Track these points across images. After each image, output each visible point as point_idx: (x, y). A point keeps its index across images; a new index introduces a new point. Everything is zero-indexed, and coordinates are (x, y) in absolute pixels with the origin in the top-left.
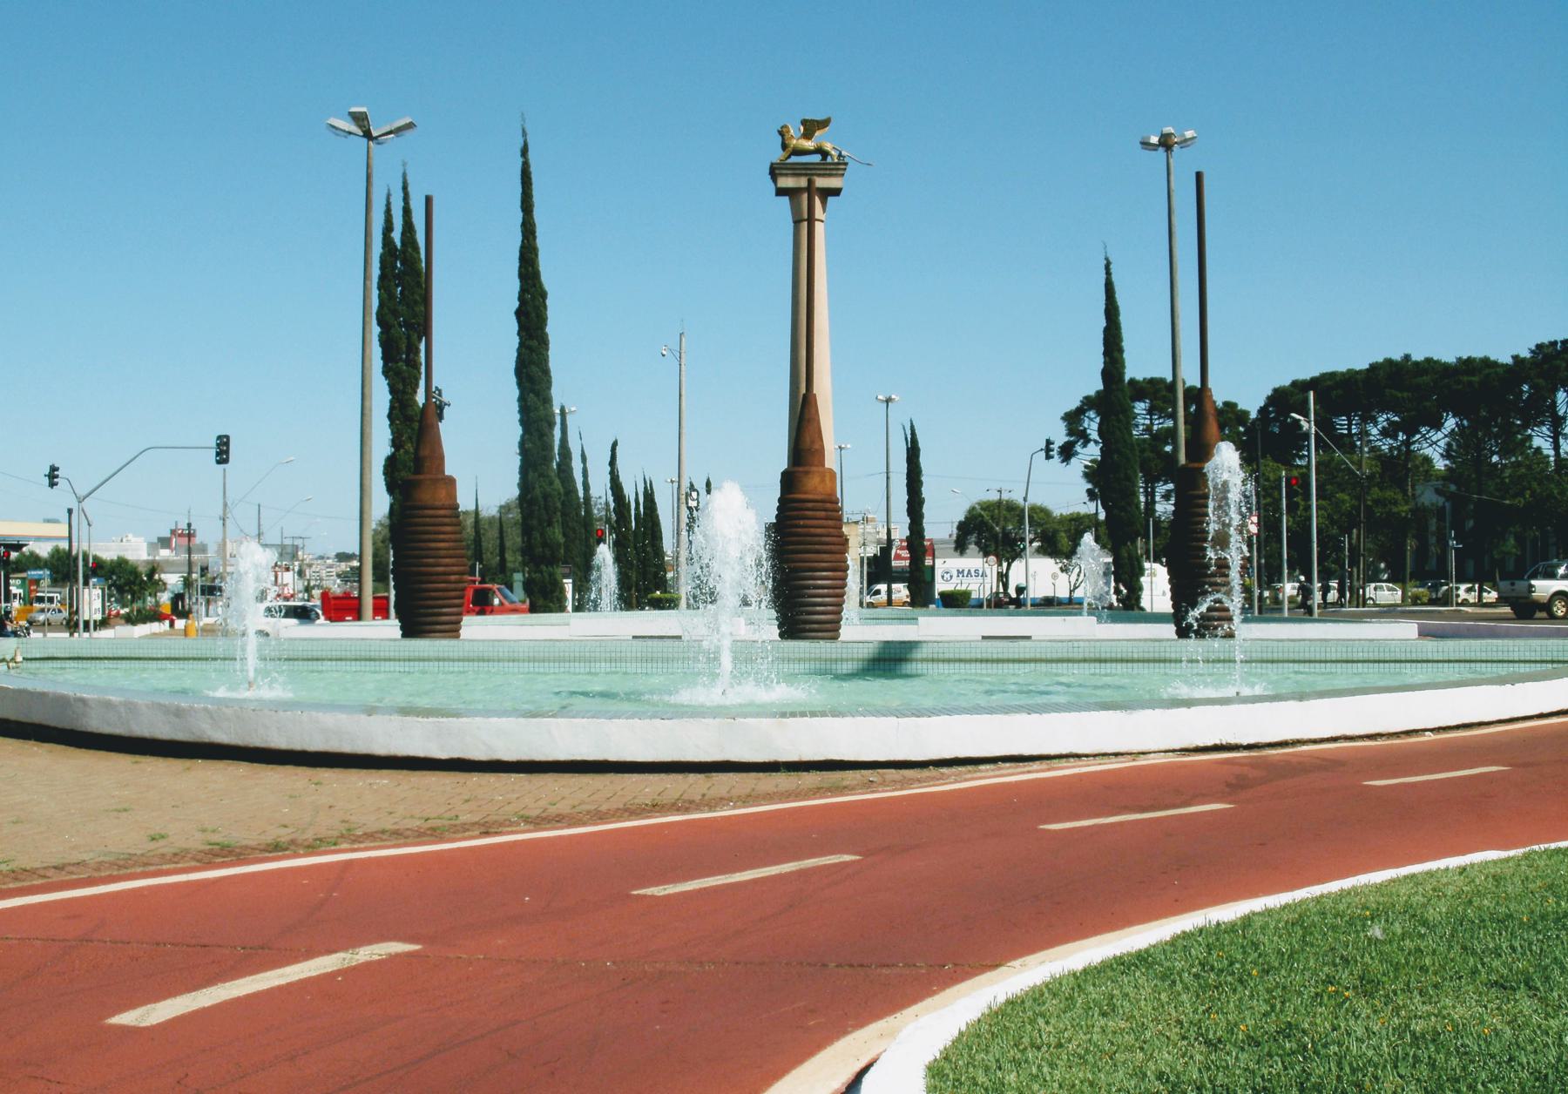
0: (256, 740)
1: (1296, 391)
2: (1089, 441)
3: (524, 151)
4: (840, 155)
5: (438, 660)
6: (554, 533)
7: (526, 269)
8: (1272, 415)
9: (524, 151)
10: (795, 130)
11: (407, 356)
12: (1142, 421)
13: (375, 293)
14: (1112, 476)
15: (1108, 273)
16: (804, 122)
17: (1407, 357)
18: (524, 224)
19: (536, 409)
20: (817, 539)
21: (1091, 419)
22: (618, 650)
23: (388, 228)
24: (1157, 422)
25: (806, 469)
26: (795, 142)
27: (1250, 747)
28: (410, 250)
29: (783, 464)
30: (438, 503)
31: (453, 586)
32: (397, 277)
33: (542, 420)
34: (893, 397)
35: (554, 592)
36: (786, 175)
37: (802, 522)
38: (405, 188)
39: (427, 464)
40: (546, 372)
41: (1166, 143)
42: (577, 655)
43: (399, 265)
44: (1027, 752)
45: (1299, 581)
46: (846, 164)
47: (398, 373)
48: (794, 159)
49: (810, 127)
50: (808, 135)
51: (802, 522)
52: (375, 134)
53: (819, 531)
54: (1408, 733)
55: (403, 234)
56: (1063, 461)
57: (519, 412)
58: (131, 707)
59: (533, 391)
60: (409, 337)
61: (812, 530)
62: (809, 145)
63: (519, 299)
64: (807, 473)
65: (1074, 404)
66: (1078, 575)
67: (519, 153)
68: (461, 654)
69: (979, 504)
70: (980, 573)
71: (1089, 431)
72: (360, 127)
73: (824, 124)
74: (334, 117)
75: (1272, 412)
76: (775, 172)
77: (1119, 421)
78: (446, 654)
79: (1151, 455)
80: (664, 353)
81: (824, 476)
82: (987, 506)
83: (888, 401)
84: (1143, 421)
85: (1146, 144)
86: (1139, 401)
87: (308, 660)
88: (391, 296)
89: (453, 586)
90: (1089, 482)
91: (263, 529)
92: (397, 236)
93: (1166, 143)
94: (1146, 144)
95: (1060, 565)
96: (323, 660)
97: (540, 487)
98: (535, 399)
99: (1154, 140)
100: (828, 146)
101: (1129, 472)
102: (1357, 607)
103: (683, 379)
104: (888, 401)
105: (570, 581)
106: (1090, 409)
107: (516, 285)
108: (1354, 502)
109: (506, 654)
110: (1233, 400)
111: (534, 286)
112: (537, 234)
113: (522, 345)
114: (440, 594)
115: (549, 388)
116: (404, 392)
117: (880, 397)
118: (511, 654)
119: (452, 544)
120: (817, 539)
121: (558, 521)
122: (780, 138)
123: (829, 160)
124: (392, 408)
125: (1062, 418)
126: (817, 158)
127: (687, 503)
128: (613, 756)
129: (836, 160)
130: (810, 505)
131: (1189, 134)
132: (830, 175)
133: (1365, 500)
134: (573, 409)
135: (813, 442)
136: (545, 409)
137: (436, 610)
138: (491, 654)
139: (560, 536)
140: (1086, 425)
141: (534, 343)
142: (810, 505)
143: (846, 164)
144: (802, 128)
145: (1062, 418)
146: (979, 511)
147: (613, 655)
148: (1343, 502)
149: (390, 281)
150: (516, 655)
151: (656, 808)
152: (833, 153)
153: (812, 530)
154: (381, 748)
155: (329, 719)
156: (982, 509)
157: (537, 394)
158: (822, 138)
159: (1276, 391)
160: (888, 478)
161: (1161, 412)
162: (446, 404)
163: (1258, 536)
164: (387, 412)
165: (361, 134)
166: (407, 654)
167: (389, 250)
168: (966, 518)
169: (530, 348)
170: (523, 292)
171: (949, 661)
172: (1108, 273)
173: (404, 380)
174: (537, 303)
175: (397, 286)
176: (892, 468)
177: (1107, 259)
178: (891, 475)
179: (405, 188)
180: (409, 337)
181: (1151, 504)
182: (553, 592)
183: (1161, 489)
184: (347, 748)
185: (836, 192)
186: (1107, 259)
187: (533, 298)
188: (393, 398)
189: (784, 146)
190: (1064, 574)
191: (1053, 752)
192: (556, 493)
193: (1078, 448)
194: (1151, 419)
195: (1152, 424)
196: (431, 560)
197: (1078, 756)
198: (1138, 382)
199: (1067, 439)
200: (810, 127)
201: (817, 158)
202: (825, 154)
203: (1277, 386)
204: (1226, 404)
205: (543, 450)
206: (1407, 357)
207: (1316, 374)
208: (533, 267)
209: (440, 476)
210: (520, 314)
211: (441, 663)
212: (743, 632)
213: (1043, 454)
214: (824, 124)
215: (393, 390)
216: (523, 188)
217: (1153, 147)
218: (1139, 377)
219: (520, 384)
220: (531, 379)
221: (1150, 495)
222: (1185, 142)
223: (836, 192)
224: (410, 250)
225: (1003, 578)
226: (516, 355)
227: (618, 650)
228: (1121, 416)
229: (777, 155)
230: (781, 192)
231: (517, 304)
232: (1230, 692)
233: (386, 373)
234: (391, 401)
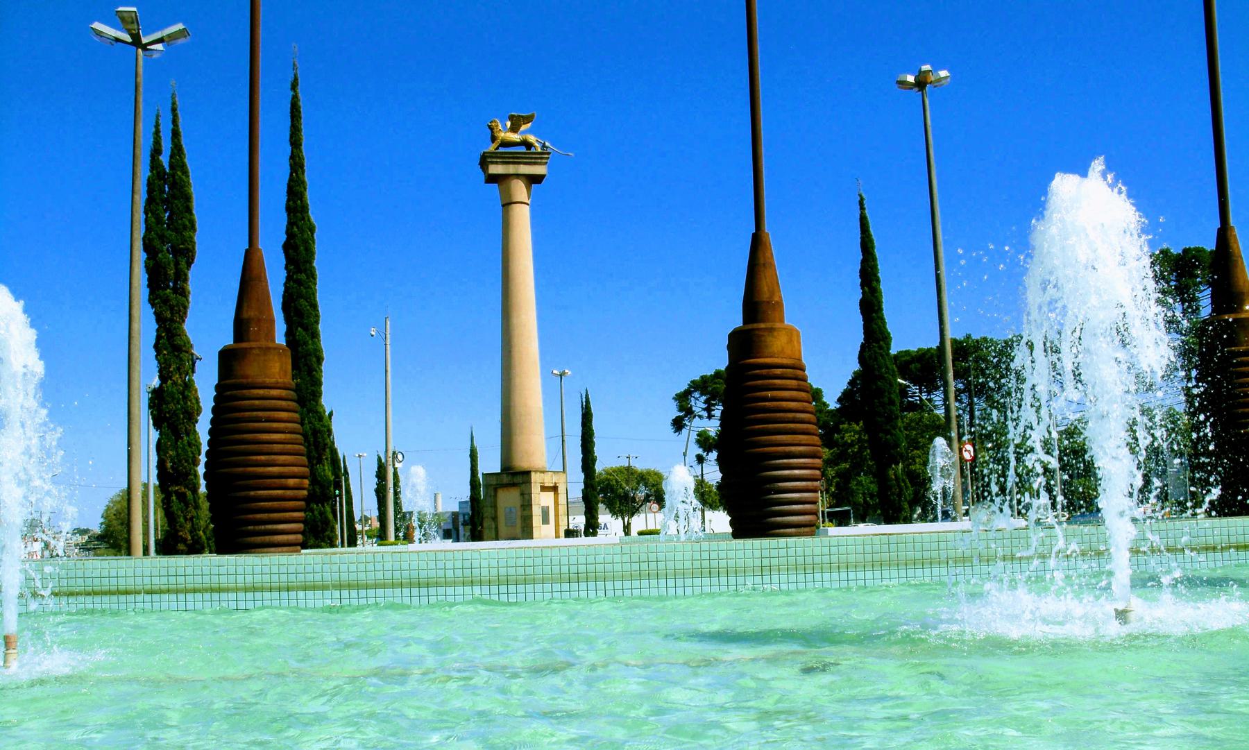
3: (294, 86)
5: (340, 587)
6: (324, 470)
7: (295, 202)
11: (175, 283)
13: (140, 216)
14: (876, 401)
15: (862, 208)
17: (968, 337)
18: (292, 157)
19: (305, 343)
20: (790, 415)
22: (653, 557)
23: (156, 151)
25: (768, 325)
28: (179, 173)
29: (736, 320)
31: (289, 493)
32: (165, 201)
33: (310, 355)
34: (566, 371)
35: (326, 530)
36: (497, 163)
37: (769, 394)
38: (174, 110)
40: (314, 306)
42: (582, 568)
43: (167, 189)
46: (549, 153)
47: (166, 301)
51: (769, 394)
52: (145, 40)
53: (793, 405)
55: (172, 157)
56: (675, 432)
60: (177, 264)
61: (784, 404)
62: (515, 137)
63: (287, 233)
64: (771, 330)
65: (683, 387)
68: (380, 575)
71: (694, 409)
72: (129, 32)
74: (100, 21)
76: (484, 161)
77: (880, 348)
78: (353, 576)
80: (373, 333)
81: (792, 334)
87: (96, 593)
88: (159, 221)
89: (289, 493)
91: (120, 44)
92: (165, 159)
94: (903, 84)
96: (137, 592)
97: (310, 423)
98: (304, 333)
99: (911, 79)
100: (532, 139)
101: (892, 396)
106: (695, 391)
109: (459, 573)
111: (303, 219)
113: (289, 278)
114: (276, 504)
115: (317, 322)
116: (172, 320)
117: (555, 372)
118: (467, 573)
119: (288, 436)
120: (790, 415)
121: (327, 459)
122: (489, 131)
124: (159, 338)
125: (674, 398)
127: (394, 465)
129: (539, 150)
130: (778, 371)
132: (535, 164)
135: (772, 293)
136: (314, 343)
137: (269, 527)
138: (432, 573)
139: (330, 474)
140: (693, 403)
141: (303, 276)
142: (778, 371)
145: (674, 398)
147: (644, 566)
149: (157, 204)
150: (476, 572)
152: (536, 144)
153: (784, 404)
157: (306, 329)
162: (197, 359)
164: (153, 342)
165: (129, 40)
166: (284, 578)
167: (158, 173)
169: (299, 282)
173: (172, 308)
174: (306, 236)
175: (165, 211)
176: (566, 432)
178: (566, 438)
179: (174, 110)
180: (177, 264)
182: (324, 530)
187: (302, 231)
188: (160, 327)
192: (325, 430)
201: (523, 149)
205: (312, 385)
206: (968, 337)
208: (302, 201)
209: (271, 345)
211: (345, 593)
215: (160, 318)
216: (292, 121)
220: (300, 314)
224: (179, 173)
226: (283, 289)
227: (653, 557)
228: (881, 343)
231: (284, 237)
233: (152, 301)
234: (158, 330)
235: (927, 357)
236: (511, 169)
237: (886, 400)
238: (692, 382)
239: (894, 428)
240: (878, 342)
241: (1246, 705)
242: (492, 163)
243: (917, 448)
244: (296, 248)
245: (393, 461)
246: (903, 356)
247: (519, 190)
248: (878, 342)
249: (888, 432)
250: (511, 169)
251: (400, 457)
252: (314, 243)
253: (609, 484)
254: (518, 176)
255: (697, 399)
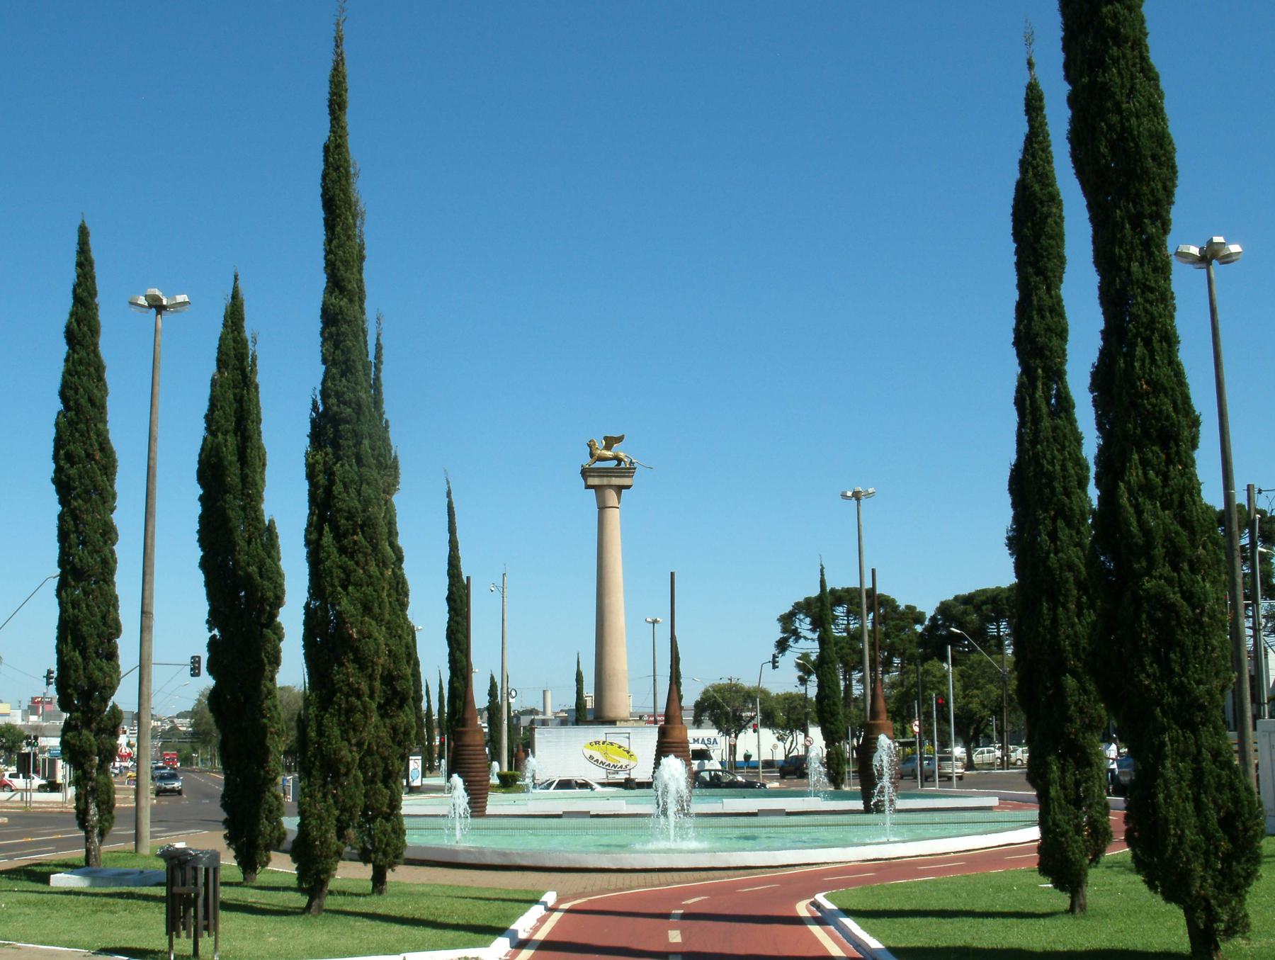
0: (540, 864)
1: (958, 604)
2: (800, 637)
3: (449, 494)
4: (631, 463)
8: (940, 622)
9: (449, 494)
10: (600, 444)
12: (841, 622)
15: (822, 574)
16: (606, 438)
18: (450, 542)
21: (801, 620)
24: (853, 622)
26: (599, 452)
27: (886, 859)
30: (472, 743)
36: (594, 476)
39: (469, 722)
41: (857, 495)
44: (811, 862)
45: (1143, 590)
46: (635, 469)
48: (599, 465)
49: (610, 442)
50: (608, 447)
54: (945, 854)
57: (449, 662)
58: (511, 854)
59: (459, 649)
62: (609, 454)
64: (672, 728)
65: (788, 608)
66: (792, 743)
67: (446, 495)
69: (711, 687)
70: (712, 741)
71: (799, 630)
73: (620, 439)
75: (940, 619)
76: (585, 473)
77: (829, 668)
79: (848, 651)
82: (719, 689)
83: (654, 622)
84: (842, 622)
85: (844, 496)
86: (839, 606)
90: (800, 671)
93: (857, 495)
94: (844, 496)
95: (777, 735)
99: (849, 494)
100: (622, 455)
102: (1003, 769)
103: (505, 608)
104: (654, 622)
105: (420, 757)
107: (445, 581)
108: (999, 692)
110: (913, 604)
111: (459, 582)
112: (459, 548)
113: (450, 619)
123: (623, 465)
125: (778, 620)
126: (613, 464)
127: (508, 700)
128: (674, 866)
131: (870, 490)
133: (1007, 690)
134: (420, 628)
140: (797, 625)
143: (635, 469)
144: (604, 443)
145: (778, 620)
146: (712, 693)
148: (991, 691)
151: (704, 880)
154: (591, 865)
155: (570, 856)
156: (714, 691)
158: (619, 450)
159: (942, 604)
160: (654, 680)
161: (856, 615)
163: (919, 733)
168: (702, 698)
170: (451, 586)
171: (757, 827)
172: (822, 574)
177: (822, 565)
178: (657, 677)
181: (848, 687)
183: (856, 675)
184: (577, 866)
185: (628, 487)
186: (822, 565)
189: (592, 455)
190: (781, 742)
191: (819, 862)
193: (791, 642)
194: (848, 620)
195: (849, 624)
196: (474, 774)
197: (828, 863)
198: (838, 591)
199: (782, 635)
200: (610, 442)
202: (620, 460)
203: (943, 600)
204: (907, 607)
207: (973, 591)
208: (457, 569)
210: (450, 599)
212: (625, 809)
213: (771, 664)
214: (620, 439)
217: (849, 498)
218: (839, 587)
219: (450, 645)
220: (459, 643)
221: (848, 680)
222: (868, 495)
223: (628, 487)
225: (733, 749)
229: (586, 461)
230: (588, 487)
232: (885, 839)
235: (999, 597)
236: (605, 481)
237: (831, 702)
238: (796, 604)
239: (836, 720)
240: (827, 664)
241: (2, 807)
242: (590, 476)
243: (977, 689)
244: (455, 601)
245: (508, 697)
246: (979, 596)
247: (611, 497)
248: (827, 664)
249: (832, 723)
250: (605, 481)
251: (513, 693)
252: (503, 793)
253: (715, 701)
254: (610, 486)
255: (801, 620)
